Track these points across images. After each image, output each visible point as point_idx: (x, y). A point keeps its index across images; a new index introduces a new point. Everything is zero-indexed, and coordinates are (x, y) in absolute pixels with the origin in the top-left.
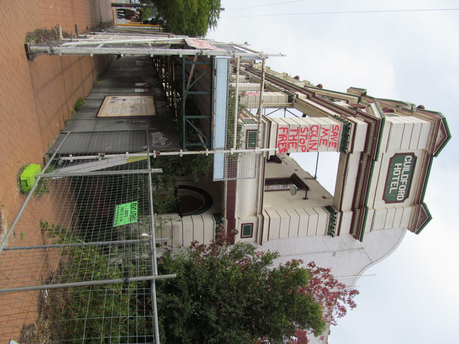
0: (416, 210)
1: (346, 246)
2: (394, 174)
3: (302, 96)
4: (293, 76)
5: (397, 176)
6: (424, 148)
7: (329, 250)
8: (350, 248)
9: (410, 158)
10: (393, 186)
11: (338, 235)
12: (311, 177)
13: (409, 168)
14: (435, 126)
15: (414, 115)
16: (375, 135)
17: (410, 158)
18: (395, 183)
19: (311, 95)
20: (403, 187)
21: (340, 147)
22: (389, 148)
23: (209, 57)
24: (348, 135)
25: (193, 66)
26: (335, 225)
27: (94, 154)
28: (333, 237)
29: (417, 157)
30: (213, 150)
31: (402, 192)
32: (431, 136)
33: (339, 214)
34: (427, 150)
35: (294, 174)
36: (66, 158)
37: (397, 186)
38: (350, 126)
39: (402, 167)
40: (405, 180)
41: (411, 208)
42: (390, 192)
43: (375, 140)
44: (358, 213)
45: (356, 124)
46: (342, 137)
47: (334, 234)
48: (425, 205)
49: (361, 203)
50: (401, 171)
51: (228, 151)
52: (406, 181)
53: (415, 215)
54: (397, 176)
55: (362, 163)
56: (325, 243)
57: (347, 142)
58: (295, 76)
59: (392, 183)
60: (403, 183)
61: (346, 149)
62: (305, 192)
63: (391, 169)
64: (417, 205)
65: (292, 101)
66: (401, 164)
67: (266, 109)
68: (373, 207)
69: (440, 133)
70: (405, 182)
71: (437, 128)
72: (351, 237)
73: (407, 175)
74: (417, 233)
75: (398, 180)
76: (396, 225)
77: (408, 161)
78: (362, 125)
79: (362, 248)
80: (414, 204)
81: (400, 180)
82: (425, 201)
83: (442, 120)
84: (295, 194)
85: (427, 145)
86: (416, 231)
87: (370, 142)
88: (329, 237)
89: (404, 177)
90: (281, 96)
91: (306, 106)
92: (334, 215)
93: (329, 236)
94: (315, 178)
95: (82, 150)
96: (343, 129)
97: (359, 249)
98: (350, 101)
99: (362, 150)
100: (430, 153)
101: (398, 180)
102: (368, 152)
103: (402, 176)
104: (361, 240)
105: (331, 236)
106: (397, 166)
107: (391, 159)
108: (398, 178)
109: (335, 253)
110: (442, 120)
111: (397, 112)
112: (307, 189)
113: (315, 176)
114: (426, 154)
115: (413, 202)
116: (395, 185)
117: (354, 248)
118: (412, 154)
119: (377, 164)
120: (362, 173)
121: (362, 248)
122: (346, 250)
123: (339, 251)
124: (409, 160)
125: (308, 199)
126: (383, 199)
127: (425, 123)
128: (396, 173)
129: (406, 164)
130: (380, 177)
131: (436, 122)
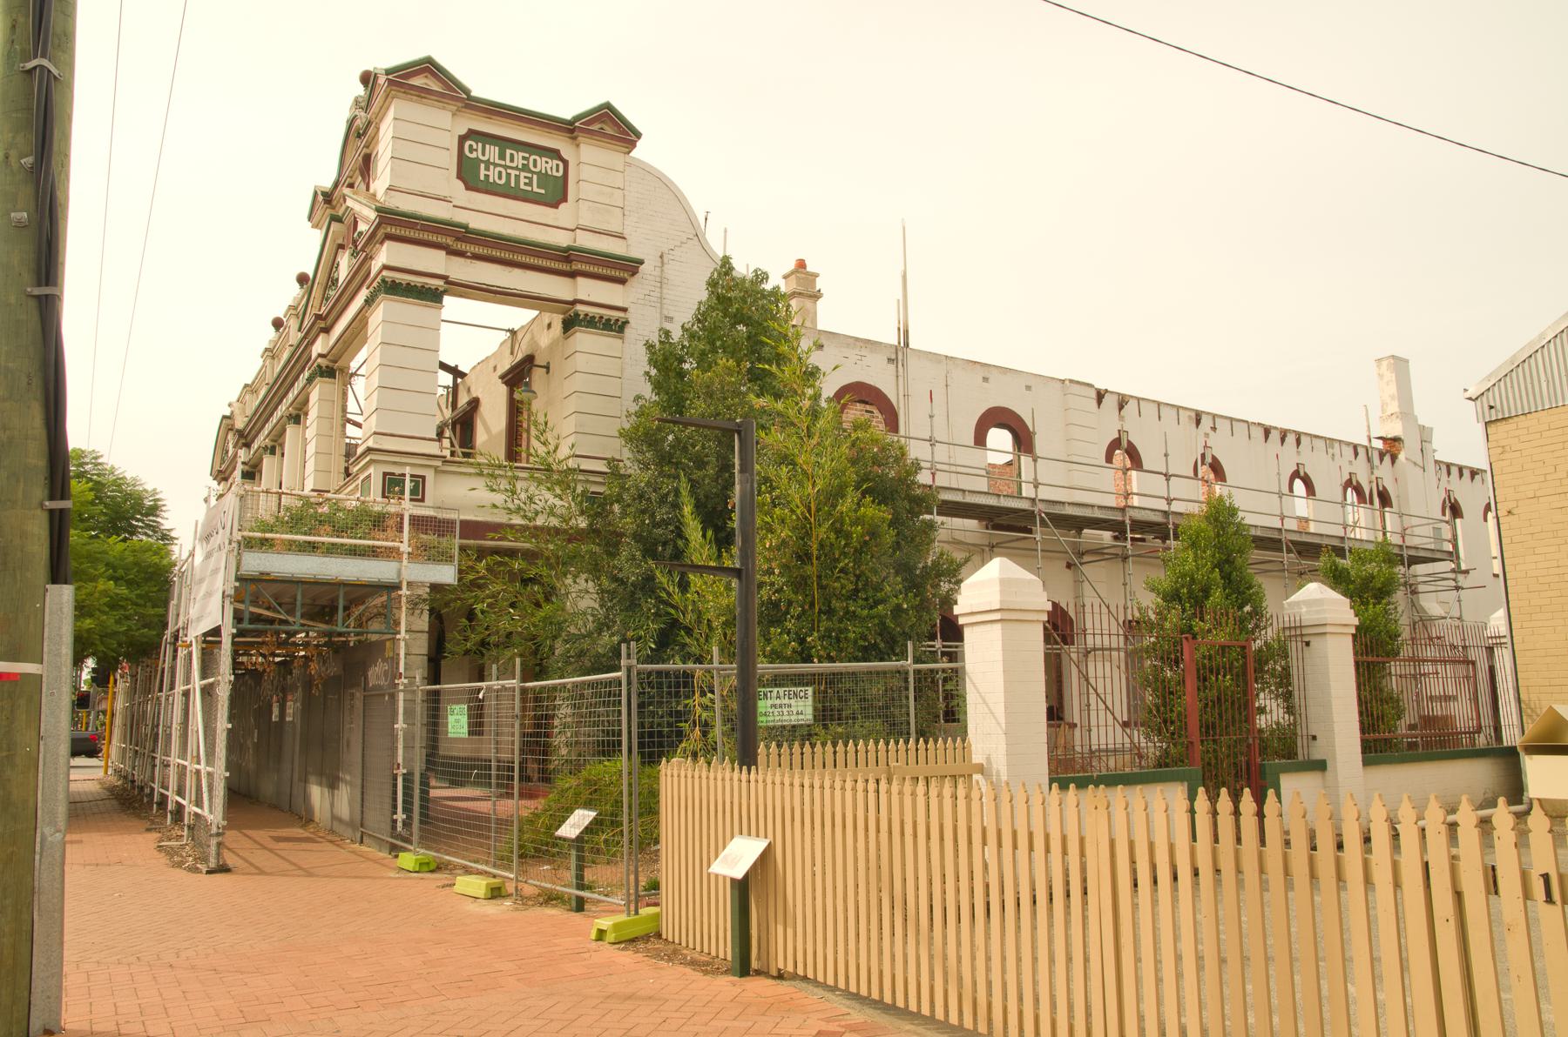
2: (503, 181)
3: (319, 347)
4: (271, 333)
5: (509, 175)
9: (471, 146)
10: (530, 184)
11: (624, 310)
16: (412, 226)
17: (471, 146)
18: (523, 181)
19: (324, 324)
20: (535, 161)
21: (432, 301)
22: (442, 193)
23: (237, 584)
24: (408, 284)
25: (252, 609)
26: (601, 317)
27: (395, 778)
28: (627, 322)
29: (469, 130)
30: (401, 582)
31: (544, 165)
33: (579, 307)
35: (502, 377)
36: (400, 824)
37: (530, 175)
38: (389, 280)
39: (488, 163)
41: (582, 146)
42: (543, 191)
45: (385, 267)
47: (621, 320)
50: (496, 165)
51: (405, 556)
52: (521, 154)
54: (509, 175)
57: (423, 287)
58: (273, 329)
59: (522, 186)
61: (437, 289)
62: (535, 368)
65: (333, 370)
66: (482, 166)
67: (348, 411)
68: (573, 230)
69: (418, 81)
70: (524, 158)
72: (634, 282)
73: (508, 152)
74: (638, 135)
75: (517, 173)
77: (476, 150)
78: (385, 255)
79: (661, 257)
80: (574, 138)
81: (516, 168)
82: (568, 116)
83: (390, 77)
84: (534, 392)
85: (444, 108)
86: (634, 138)
88: (628, 331)
89: (512, 160)
90: (320, 395)
91: (345, 342)
92: (581, 317)
93: (626, 330)
94: (513, 332)
95: (388, 801)
97: (662, 263)
98: (340, 241)
99: (444, 253)
101: (517, 173)
103: (508, 163)
104: (641, 262)
107: (468, 188)
108: (513, 173)
109: (666, 317)
110: (390, 77)
111: (371, 147)
112: (529, 359)
113: (509, 330)
116: (527, 181)
118: (462, 139)
119: (477, 223)
123: (661, 308)
124: (475, 147)
125: (548, 363)
126: (557, 208)
127: (395, 112)
128: (500, 178)
129: (483, 154)
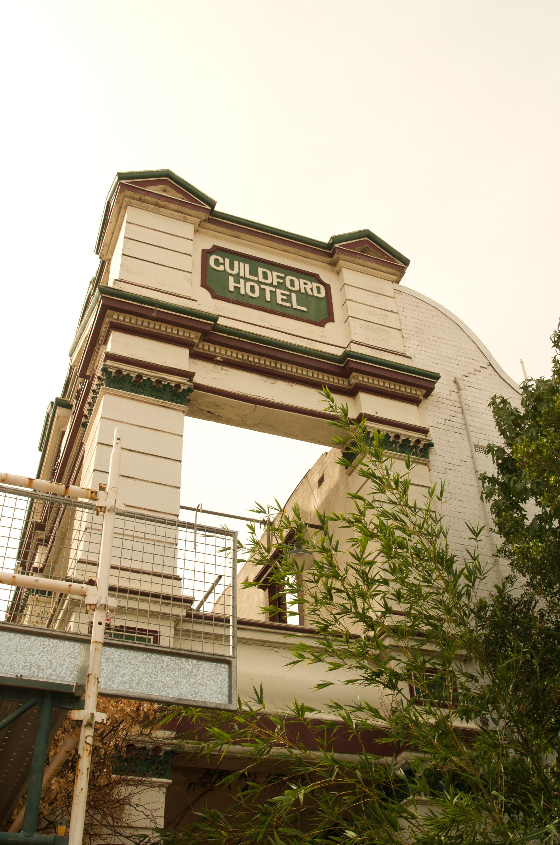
0: (348, 258)
1: (453, 419)
5: (263, 291)
6: (191, 228)
7: (470, 460)
8: (460, 410)
10: (289, 300)
11: (425, 431)
12: (266, 537)
13: (242, 264)
14: (138, 196)
15: (109, 256)
21: (172, 400)
26: (397, 436)
28: (431, 445)
29: (214, 246)
30: (81, 688)
32: (161, 209)
34: (198, 221)
37: (288, 293)
39: (237, 278)
40: (274, 277)
43: (160, 316)
44: (361, 379)
46: (141, 393)
48: (336, 239)
49: (333, 369)
50: (247, 280)
52: (275, 274)
53: (362, 262)
54: (263, 291)
55: (222, 358)
56: (451, 467)
59: (279, 301)
60: (281, 281)
63: (241, 299)
64: (336, 256)
66: (231, 279)
70: (278, 277)
71: (143, 193)
72: (426, 403)
74: (406, 262)
75: (273, 289)
76: (390, 305)
81: (271, 285)
82: (326, 240)
83: (123, 182)
85: (185, 220)
87: (163, 328)
96: (120, 388)
100: (204, 216)
101: (273, 289)
102: (192, 336)
103: (261, 279)
104: (436, 377)
105: (432, 450)
106: (235, 287)
108: (268, 289)
110: (123, 182)
114: (207, 225)
115: (329, 267)
117: (457, 399)
120: (251, 359)
121: (455, 382)
122: (464, 419)
124: (221, 260)
126: (323, 326)
129: (232, 268)
130: (263, 325)
131: (128, 193)
